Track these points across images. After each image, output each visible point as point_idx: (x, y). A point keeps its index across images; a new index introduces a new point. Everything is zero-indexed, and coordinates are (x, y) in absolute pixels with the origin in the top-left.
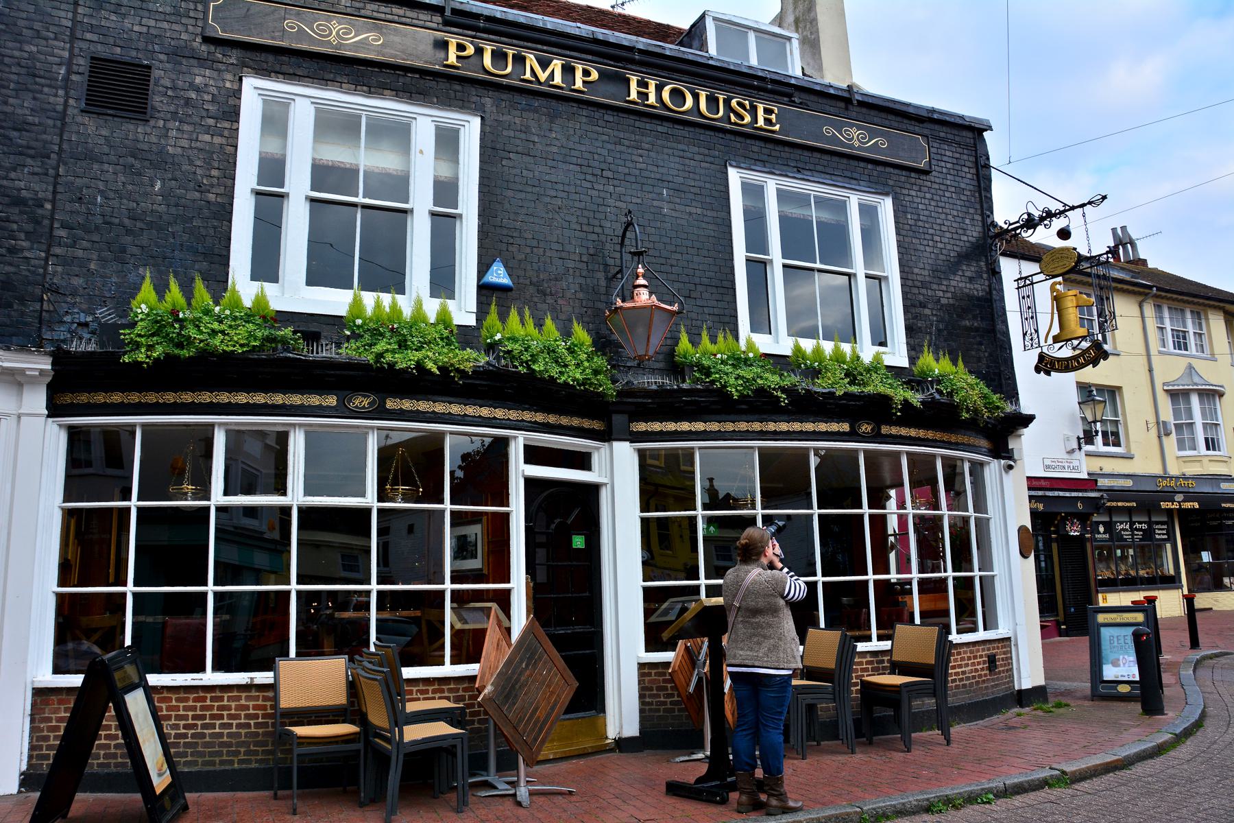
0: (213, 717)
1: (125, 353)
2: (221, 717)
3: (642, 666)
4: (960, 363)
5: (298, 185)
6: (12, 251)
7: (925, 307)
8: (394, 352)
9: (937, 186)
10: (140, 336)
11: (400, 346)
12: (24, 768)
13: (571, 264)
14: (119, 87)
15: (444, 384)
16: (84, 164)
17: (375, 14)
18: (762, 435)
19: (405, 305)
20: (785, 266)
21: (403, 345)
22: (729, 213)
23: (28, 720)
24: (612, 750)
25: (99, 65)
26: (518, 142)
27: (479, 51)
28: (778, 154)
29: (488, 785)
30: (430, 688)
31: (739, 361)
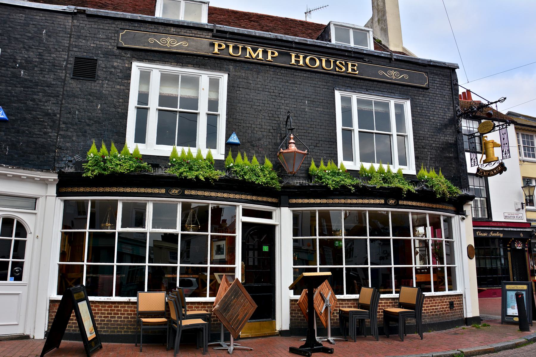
0: (115, 314)
1: (84, 173)
2: (118, 314)
3: (291, 301)
4: (440, 172)
5: (153, 104)
6: (45, 133)
7: (424, 148)
8: (187, 172)
9: (432, 94)
10: (90, 166)
11: (190, 169)
12: (46, 330)
13: (265, 134)
14: (85, 68)
15: (207, 185)
16: (72, 99)
17: (185, 34)
18: (345, 205)
19: (194, 151)
20: (359, 132)
21: (191, 169)
22: (335, 110)
23: (48, 312)
24: (277, 335)
25: (78, 60)
26: (243, 83)
27: (227, 47)
28: (358, 84)
29: (220, 345)
30: (200, 306)
31: (335, 173)
